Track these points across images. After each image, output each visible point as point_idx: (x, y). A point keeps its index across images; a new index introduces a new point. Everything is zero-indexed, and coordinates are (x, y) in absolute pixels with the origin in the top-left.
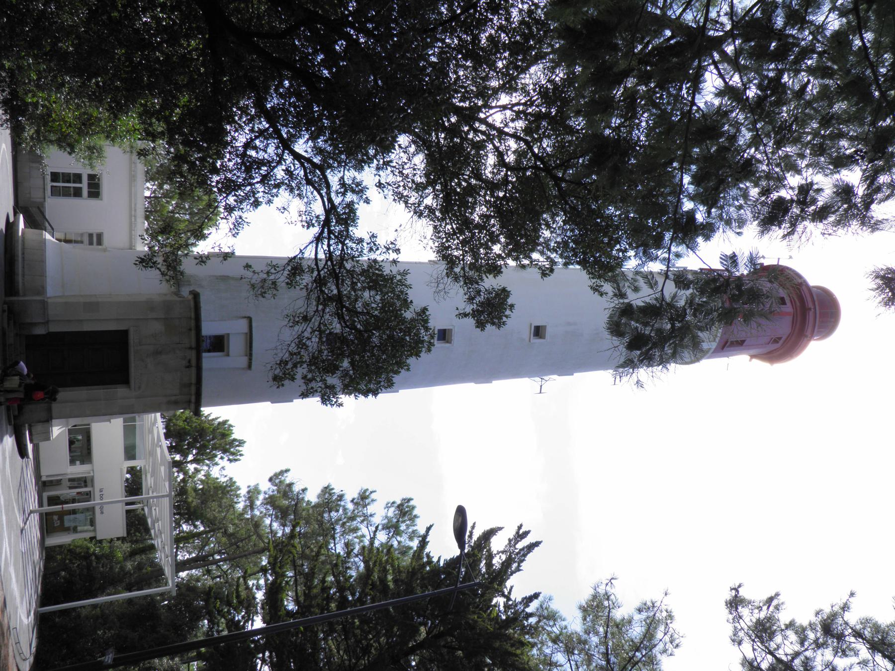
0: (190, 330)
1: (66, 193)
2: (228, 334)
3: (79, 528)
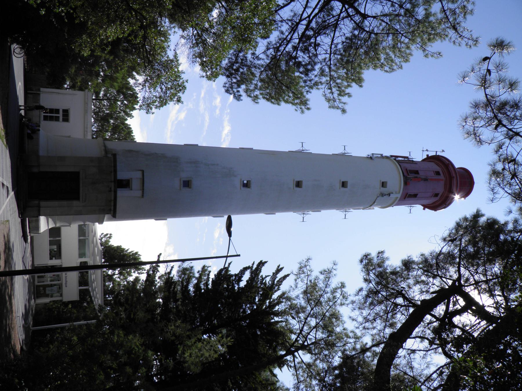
0: (111, 172)
1: (51, 119)
2: (132, 179)
3: (54, 295)
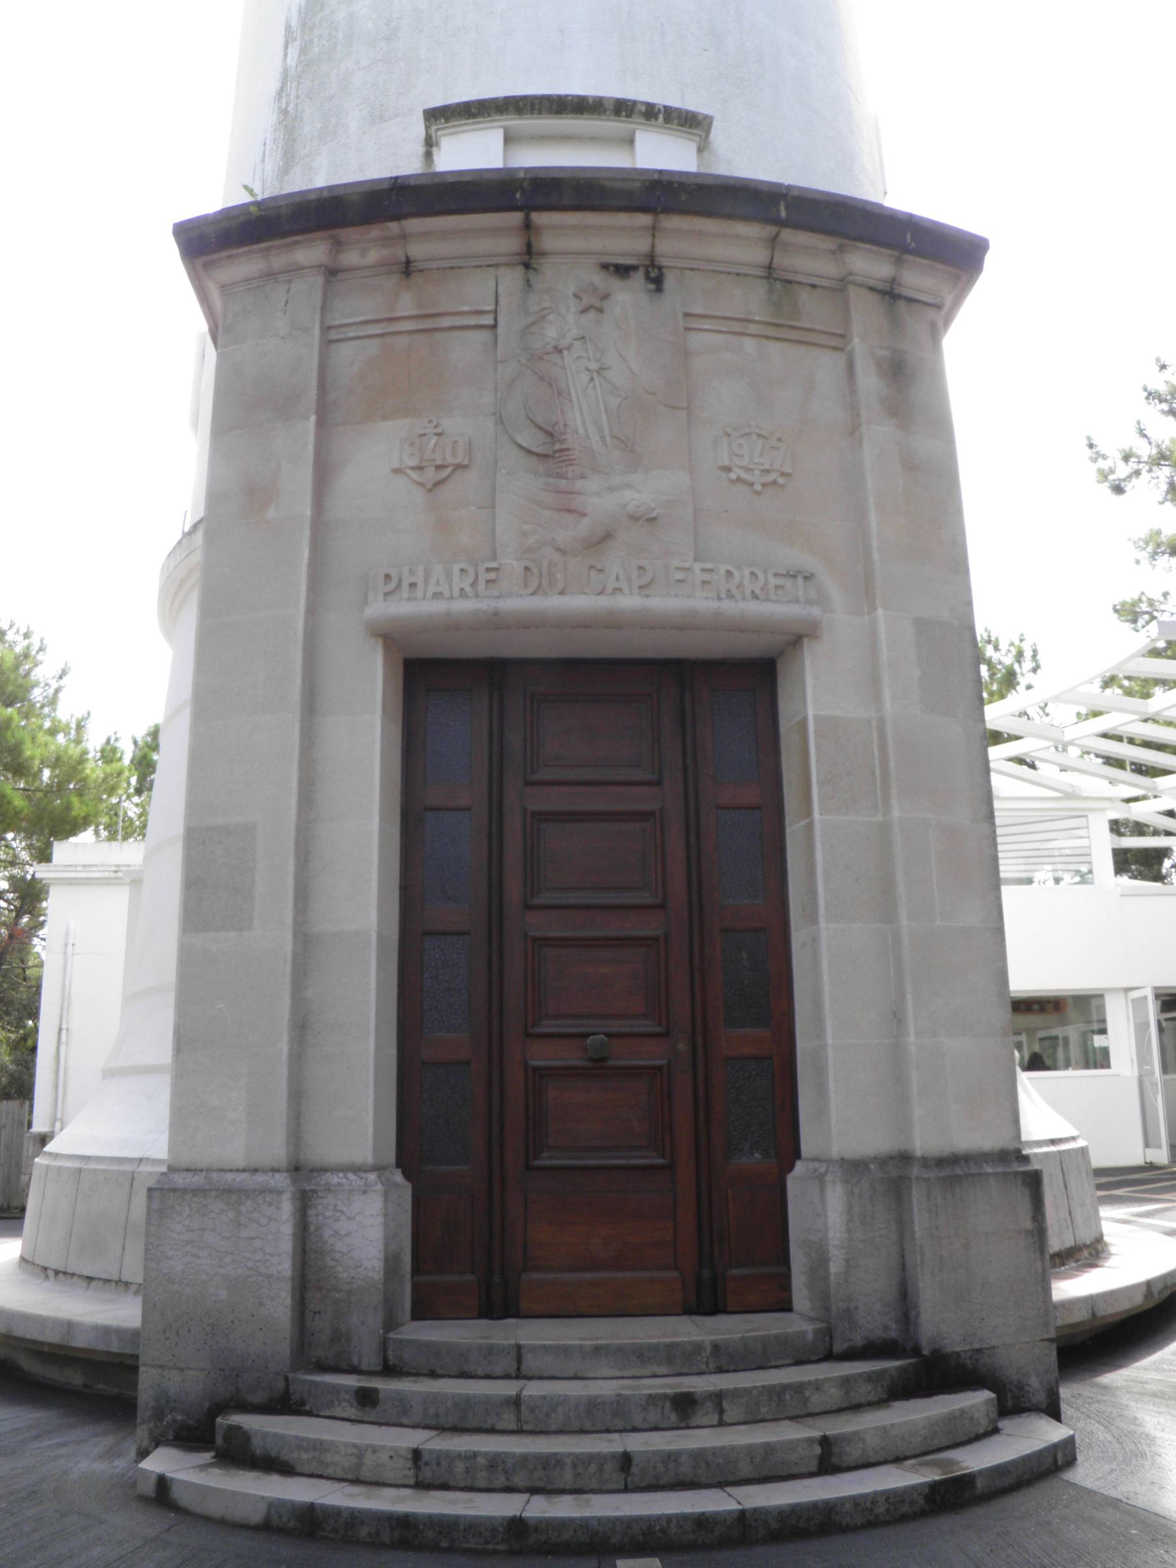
0: (407, 268)
